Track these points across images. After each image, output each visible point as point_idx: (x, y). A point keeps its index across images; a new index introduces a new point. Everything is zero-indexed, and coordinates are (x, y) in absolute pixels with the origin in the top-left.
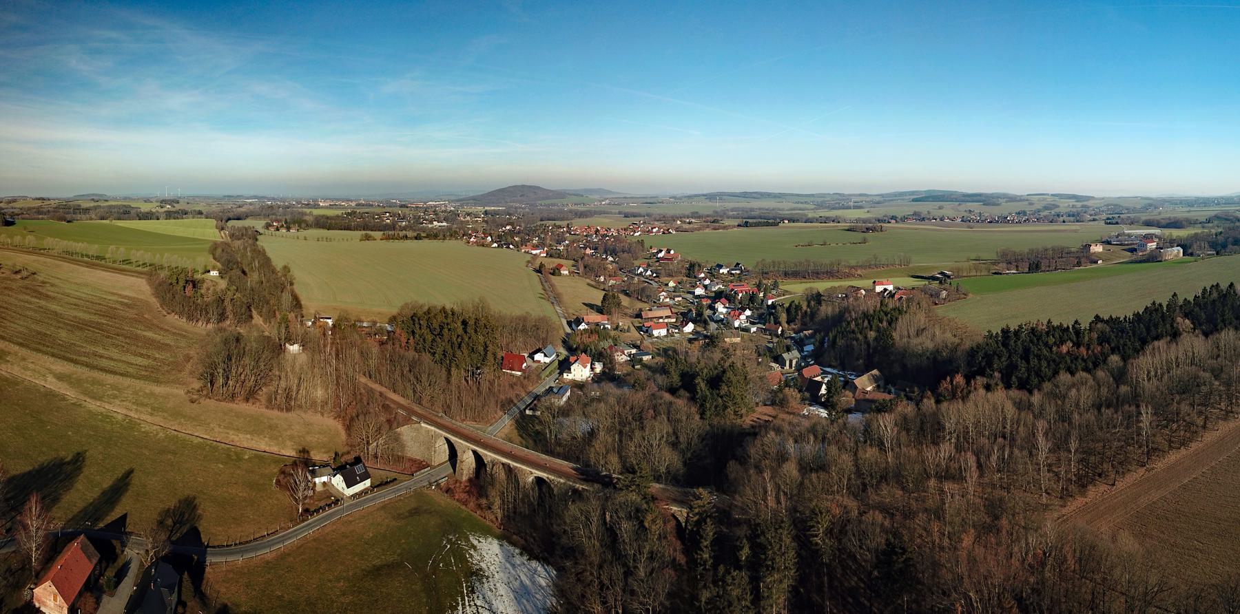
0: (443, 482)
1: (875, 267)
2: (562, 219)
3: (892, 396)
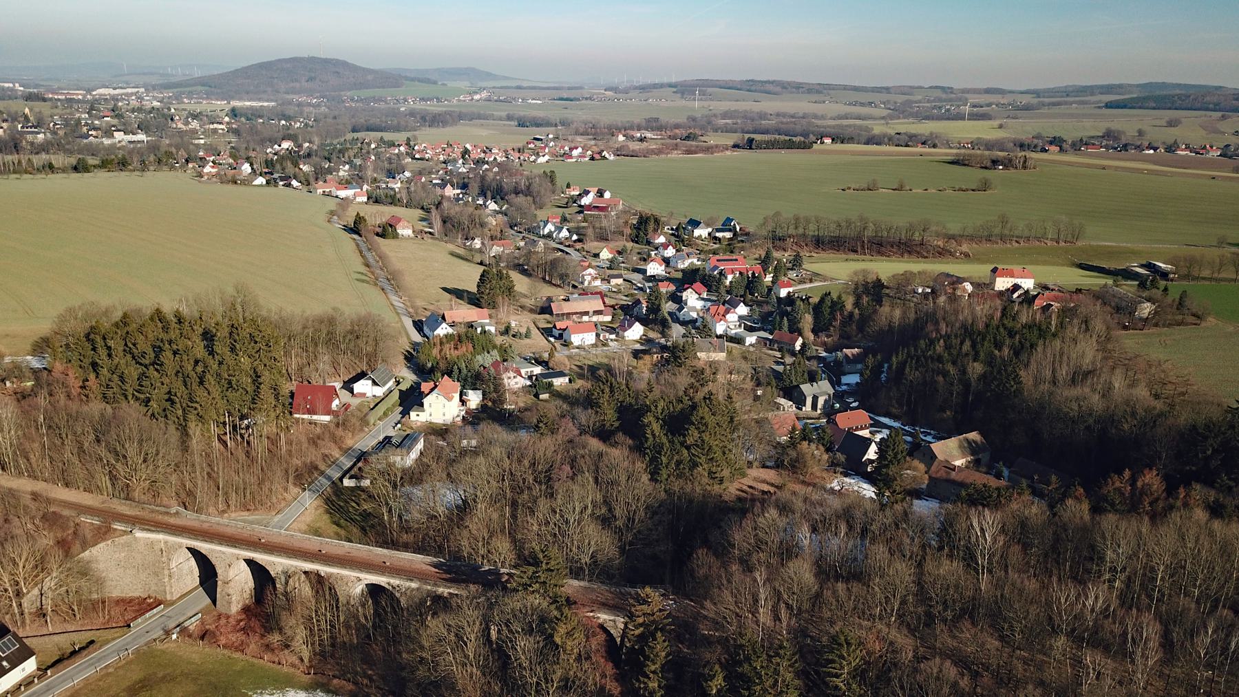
0: (193, 624)
1: (998, 239)
2: (397, 129)
3: (1003, 483)
